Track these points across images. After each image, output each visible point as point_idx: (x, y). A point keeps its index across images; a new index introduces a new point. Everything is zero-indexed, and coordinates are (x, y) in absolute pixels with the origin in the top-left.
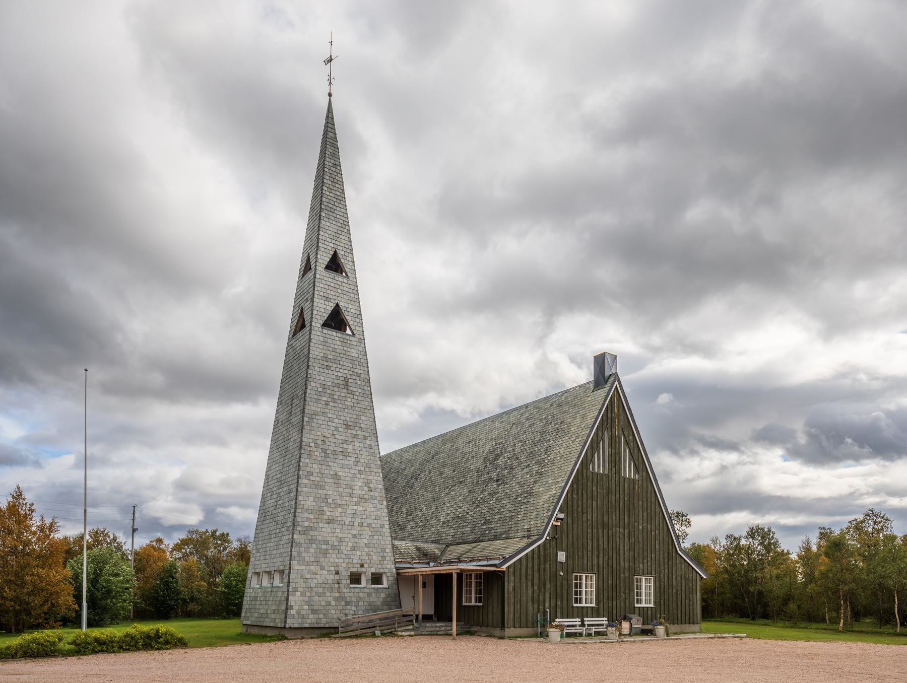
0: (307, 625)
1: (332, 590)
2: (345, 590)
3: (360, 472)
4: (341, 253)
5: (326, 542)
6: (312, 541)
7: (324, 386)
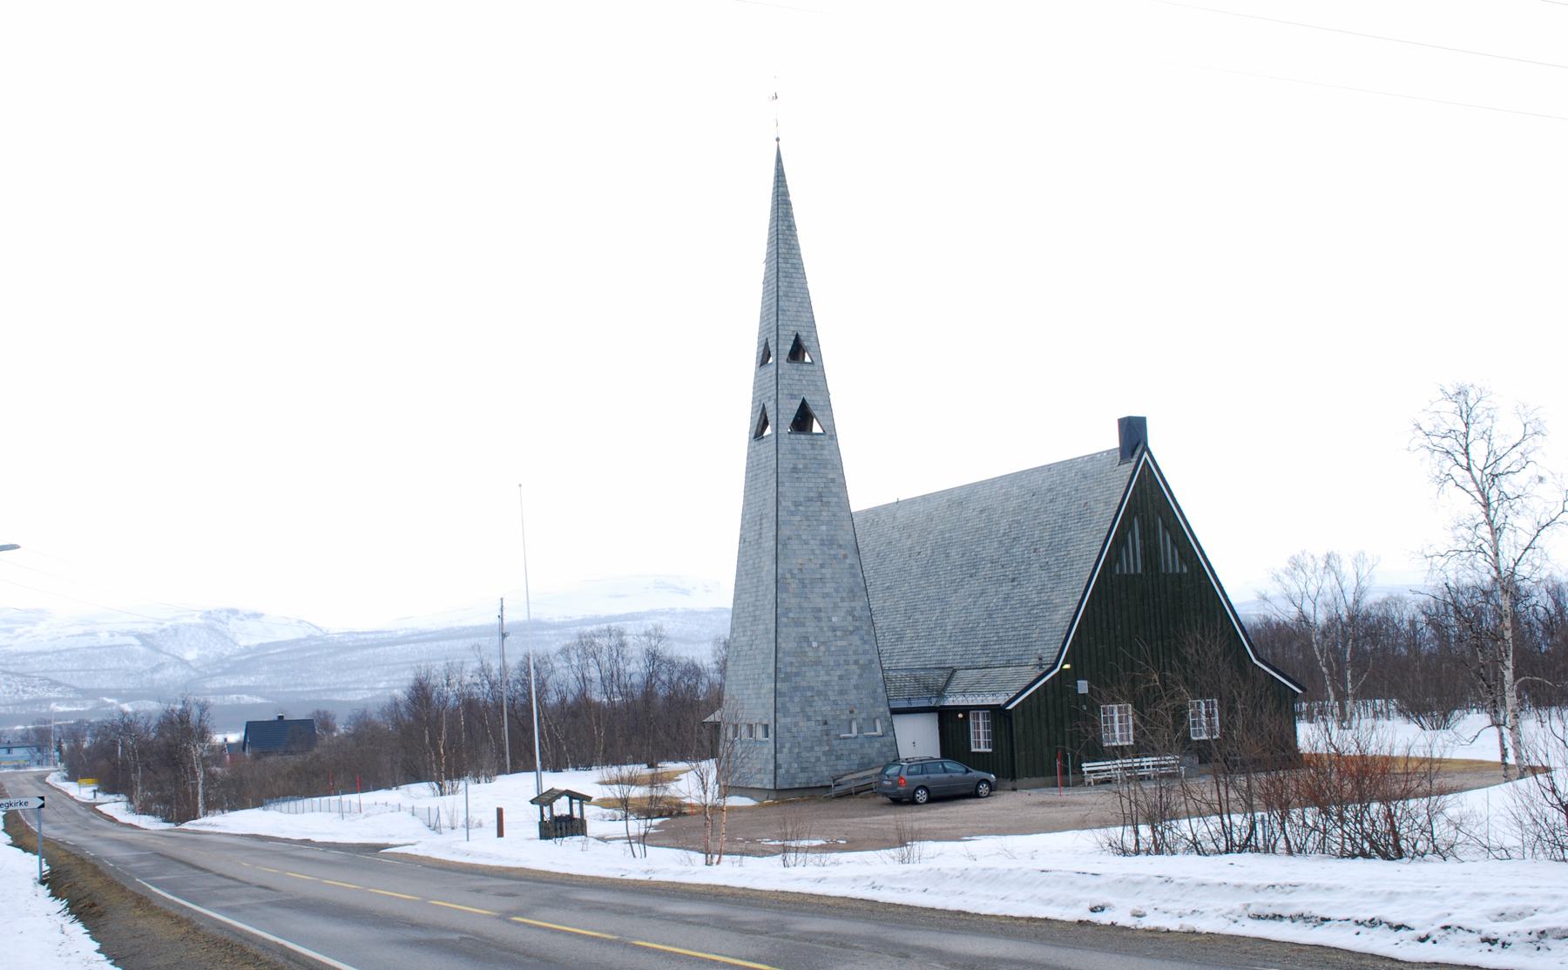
1: (820, 742)
2: (835, 743)
3: (843, 599)
4: (803, 335)
5: (811, 688)
6: (796, 689)
7: (797, 504)
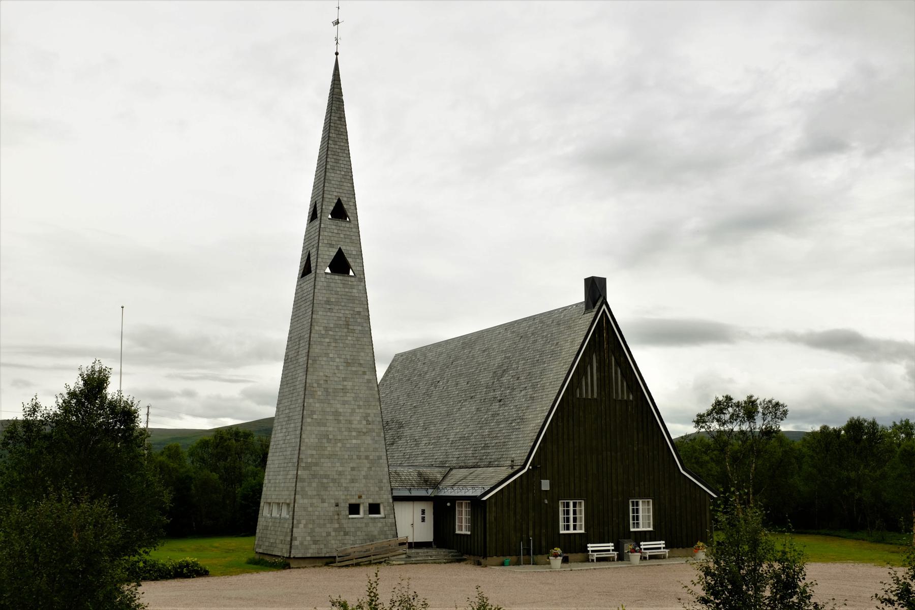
0: (309, 555)
